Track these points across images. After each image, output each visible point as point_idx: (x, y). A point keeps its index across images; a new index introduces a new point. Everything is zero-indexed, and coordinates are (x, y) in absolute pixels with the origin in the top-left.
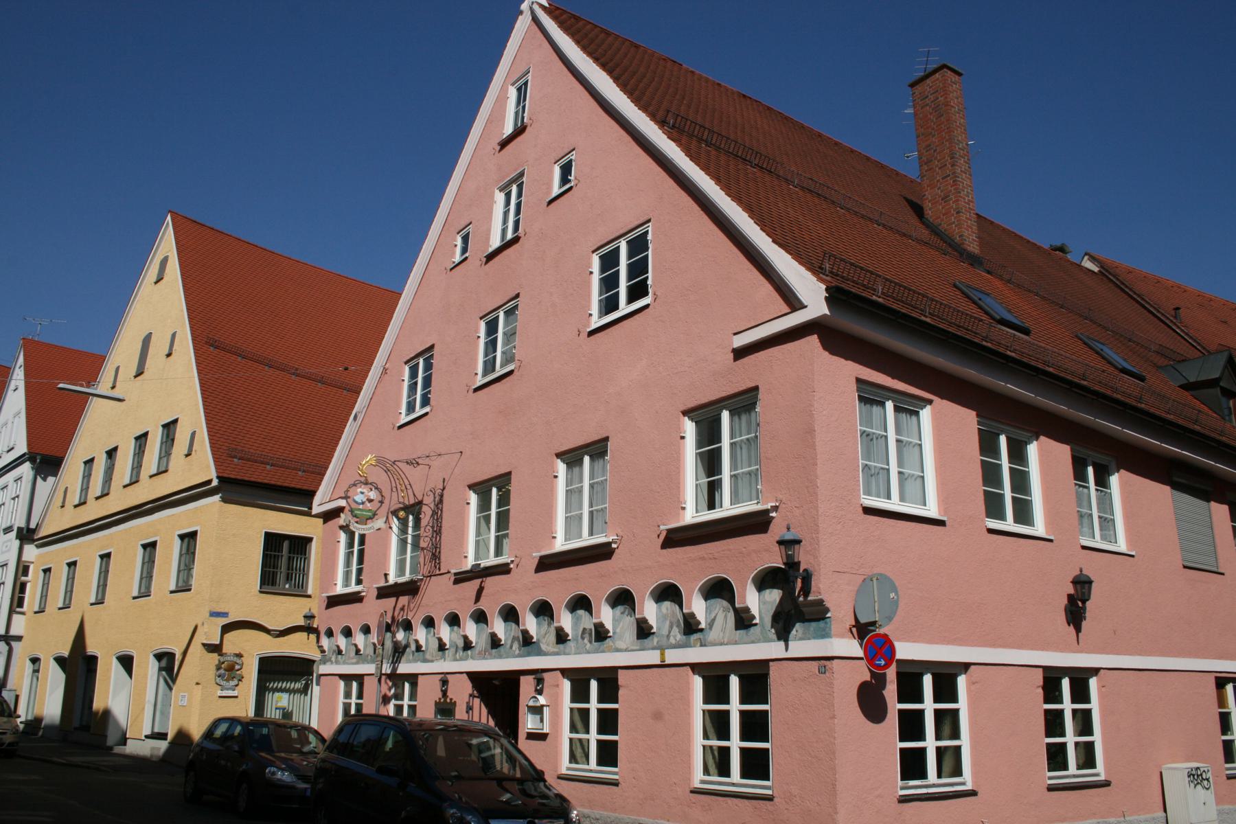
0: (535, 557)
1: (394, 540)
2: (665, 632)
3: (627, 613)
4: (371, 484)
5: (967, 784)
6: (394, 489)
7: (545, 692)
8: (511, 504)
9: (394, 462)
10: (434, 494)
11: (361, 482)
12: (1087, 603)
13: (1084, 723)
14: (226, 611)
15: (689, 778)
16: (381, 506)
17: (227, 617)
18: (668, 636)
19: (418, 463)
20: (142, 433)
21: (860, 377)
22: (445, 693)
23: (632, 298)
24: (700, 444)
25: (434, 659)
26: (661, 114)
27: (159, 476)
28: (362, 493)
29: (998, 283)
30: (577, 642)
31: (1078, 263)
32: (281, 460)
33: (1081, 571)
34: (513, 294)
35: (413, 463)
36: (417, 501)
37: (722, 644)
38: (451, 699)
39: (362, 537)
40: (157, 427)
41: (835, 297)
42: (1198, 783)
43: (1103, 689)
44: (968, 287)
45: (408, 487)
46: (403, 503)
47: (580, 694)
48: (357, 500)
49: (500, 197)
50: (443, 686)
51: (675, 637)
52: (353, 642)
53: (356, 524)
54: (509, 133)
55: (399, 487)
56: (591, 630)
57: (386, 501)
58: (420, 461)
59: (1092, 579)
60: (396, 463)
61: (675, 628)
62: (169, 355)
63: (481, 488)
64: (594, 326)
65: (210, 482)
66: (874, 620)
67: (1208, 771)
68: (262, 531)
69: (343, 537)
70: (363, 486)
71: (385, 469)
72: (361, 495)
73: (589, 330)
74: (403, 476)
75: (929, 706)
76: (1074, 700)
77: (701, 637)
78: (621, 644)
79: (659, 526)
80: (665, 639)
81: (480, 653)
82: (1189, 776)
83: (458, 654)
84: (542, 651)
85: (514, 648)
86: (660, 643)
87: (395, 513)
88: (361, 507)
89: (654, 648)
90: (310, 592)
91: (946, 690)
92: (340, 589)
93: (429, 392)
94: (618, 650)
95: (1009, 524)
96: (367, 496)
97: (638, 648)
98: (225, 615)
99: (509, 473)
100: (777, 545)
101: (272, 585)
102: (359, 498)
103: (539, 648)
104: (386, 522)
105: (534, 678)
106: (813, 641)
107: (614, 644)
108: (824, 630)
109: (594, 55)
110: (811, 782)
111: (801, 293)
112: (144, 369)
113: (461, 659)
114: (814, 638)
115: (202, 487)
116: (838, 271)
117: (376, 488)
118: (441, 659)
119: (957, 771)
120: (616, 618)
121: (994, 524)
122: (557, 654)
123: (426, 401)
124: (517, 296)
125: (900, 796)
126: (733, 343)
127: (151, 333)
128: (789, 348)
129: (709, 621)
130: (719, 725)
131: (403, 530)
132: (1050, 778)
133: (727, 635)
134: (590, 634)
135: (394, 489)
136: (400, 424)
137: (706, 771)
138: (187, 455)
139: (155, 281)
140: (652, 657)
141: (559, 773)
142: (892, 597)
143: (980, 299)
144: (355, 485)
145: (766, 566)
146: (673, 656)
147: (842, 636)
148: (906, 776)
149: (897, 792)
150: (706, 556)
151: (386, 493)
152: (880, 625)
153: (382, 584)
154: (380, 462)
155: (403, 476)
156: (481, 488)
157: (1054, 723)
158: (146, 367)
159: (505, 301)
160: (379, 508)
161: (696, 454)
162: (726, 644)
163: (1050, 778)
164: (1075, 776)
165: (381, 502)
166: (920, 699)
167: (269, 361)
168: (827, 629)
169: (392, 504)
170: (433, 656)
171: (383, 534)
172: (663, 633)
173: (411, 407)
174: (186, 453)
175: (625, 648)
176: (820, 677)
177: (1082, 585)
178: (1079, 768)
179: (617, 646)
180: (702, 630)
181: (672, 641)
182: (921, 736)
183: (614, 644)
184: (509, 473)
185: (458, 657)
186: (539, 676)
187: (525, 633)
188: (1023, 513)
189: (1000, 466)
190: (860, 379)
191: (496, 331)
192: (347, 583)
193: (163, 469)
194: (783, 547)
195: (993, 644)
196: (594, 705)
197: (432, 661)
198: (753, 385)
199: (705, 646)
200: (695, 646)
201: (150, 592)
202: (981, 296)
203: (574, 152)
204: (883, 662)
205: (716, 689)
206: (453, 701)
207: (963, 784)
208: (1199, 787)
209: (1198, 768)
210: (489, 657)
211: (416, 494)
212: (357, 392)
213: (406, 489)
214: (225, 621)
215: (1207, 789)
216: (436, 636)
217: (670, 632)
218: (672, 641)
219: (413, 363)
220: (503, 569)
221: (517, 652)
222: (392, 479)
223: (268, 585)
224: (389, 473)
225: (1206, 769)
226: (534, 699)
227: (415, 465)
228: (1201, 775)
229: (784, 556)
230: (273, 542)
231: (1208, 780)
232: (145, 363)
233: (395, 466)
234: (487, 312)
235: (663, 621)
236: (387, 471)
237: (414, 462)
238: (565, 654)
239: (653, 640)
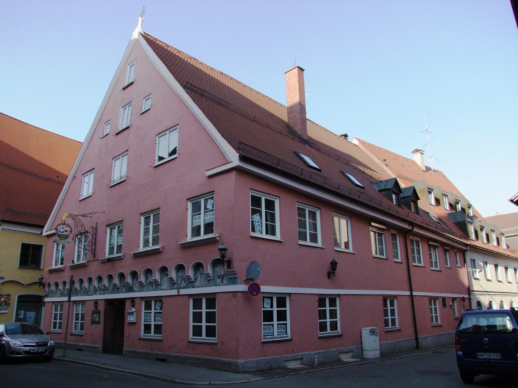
2: (179, 283)
3: (165, 275)
4: (67, 224)
5: (289, 337)
6: (76, 227)
8: (123, 232)
9: (76, 216)
10: (93, 229)
11: (62, 224)
12: (336, 271)
13: (333, 314)
15: (188, 337)
17: (4, 279)
18: (181, 284)
19: (86, 216)
22: (96, 307)
26: (185, 84)
28: (63, 228)
31: (351, 141)
32: (30, 213)
33: (334, 259)
34: (126, 150)
35: (84, 216)
36: (86, 231)
37: (200, 287)
41: (242, 158)
42: (373, 334)
43: (341, 302)
45: (82, 226)
46: (80, 232)
48: (61, 231)
50: (132, 304)
51: (183, 284)
52: (103, 284)
53: (60, 241)
54: (126, 85)
55: (78, 225)
56: (152, 282)
57: (73, 231)
59: (337, 262)
60: (77, 216)
61: (183, 281)
63: (146, 215)
64: (156, 165)
66: (252, 278)
67: (377, 330)
74: (80, 221)
75: (328, 308)
76: (391, 306)
77: (192, 284)
78: (163, 287)
79: (177, 242)
80: (179, 285)
81: (110, 291)
82: (370, 332)
83: (101, 292)
84: (134, 290)
85: (123, 290)
88: (62, 234)
89: (175, 289)
91: (333, 302)
94: (162, 290)
95: (308, 243)
102: (62, 230)
104: (73, 240)
109: (161, 57)
113: (103, 294)
116: (249, 148)
117: (69, 226)
118: (95, 294)
121: (301, 242)
122: (140, 291)
125: (263, 342)
126: (206, 174)
130: (197, 317)
131: (147, 223)
132: (320, 334)
133: (202, 283)
134: (152, 284)
135: (76, 227)
141: (140, 337)
144: (60, 225)
146: (183, 292)
147: (241, 284)
149: (262, 340)
151: (73, 228)
154: (70, 216)
155: (80, 221)
156: (146, 215)
157: (322, 315)
160: (70, 234)
162: (201, 287)
163: (320, 334)
164: (329, 333)
165: (71, 232)
167: (25, 171)
169: (75, 232)
170: (92, 293)
175: (165, 289)
177: (334, 264)
178: (331, 330)
179: (162, 288)
181: (182, 286)
187: (171, 279)
188: (314, 238)
192: (56, 265)
194: (220, 251)
195: (301, 286)
197: (91, 295)
199: (194, 288)
200: (190, 288)
203: (151, 95)
204: (256, 293)
205: (197, 304)
207: (287, 337)
208: (374, 335)
209: (373, 329)
211: (85, 228)
212: (64, 184)
213: (81, 226)
214: (2, 281)
215: (376, 336)
216: (93, 285)
217: (181, 282)
218: (182, 286)
220: (119, 259)
221: (125, 291)
224: (74, 220)
225: (376, 329)
226: (130, 309)
227: (85, 217)
228: (375, 331)
229: (221, 254)
231: (377, 333)
233: (77, 217)
238: (143, 291)
239: (175, 286)
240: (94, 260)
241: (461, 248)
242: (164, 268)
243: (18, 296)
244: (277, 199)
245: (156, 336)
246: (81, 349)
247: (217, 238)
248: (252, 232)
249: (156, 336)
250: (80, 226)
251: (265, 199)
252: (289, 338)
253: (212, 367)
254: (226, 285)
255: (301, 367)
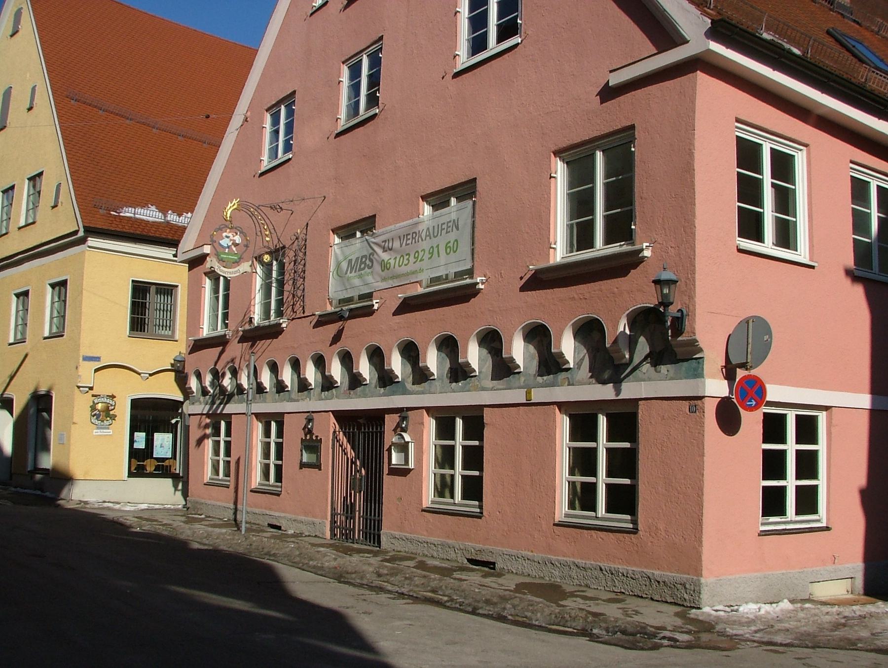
0: (400, 298)
1: (258, 282)
7: (410, 428)
14: (98, 355)
16: (246, 250)
20: (9, 186)
21: (739, 117)
23: (501, 39)
24: (572, 184)
25: (300, 398)
27: (27, 227)
28: (228, 237)
29: (867, 34)
30: (443, 381)
34: (376, 38)
38: (317, 437)
39: (227, 282)
40: (24, 181)
44: (843, 35)
45: (272, 231)
47: (445, 430)
48: (222, 244)
49: (268, 119)
58: (283, 206)
62: (30, 109)
65: (76, 232)
68: (129, 280)
69: (208, 283)
70: (228, 230)
71: (250, 213)
72: (228, 239)
73: (455, 71)
77: (569, 376)
86: (526, 382)
87: (259, 259)
90: (177, 338)
92: (205, 332)
93: (292, 138)
96: (231, 240)
97: (505, 387)
98: (97, 359)
99: (375, 216)
100: (653, 284)
101: (141, 331)
103: (404, 387)
104: (251, 266)
105: (399, 416)
106: (684, 381)
107: (480, 383)
108: (695, 370)
110: (678, 517)
111: (680, 24)
112: (6, 123)
113: (326, 399)
114: (686, 378)
115: (72, 237)
119: (814, 510)
120: (483, 358)
123: (288, 148)
124: (381, 38)
127: (11, 87)
128: (669, 86)
129: (577, 360)
135: (259, 234)
136: (262, 171)
137: (572, 506)
138: (53, 207)
139: (10, 33)
140: (518, 396)
142: (765, 339)
143: (854, 46)
145: (639, 306)
146: (538, 395)
147: (713, 377)
148: (766, 512)
150: (576, 296)
152: (751, 367)
153: (247, 327)
158: (8, 122)
159: (368, 44)
161: (568, 194)
165: (247, 246)
166: (783, 441)
168: (700, 369)
171: (247, 277)
172: (530, 372)
173: (274, 152)
174: (53, 204)
176: (690, 415)
180: (568, 369)
182: (782, 476)
183: (480, 383)
184: (375, 216)
185: (323, 397)
186: (404, 414)
189: (869, 215)
190: (739, 119)
191: (359, 75)
193: (31, 221)
196: (459, 442)
197: (298, 401)
198: (629, 124)
199: (573, 385)
201: (26, 339)
202: (854, 43)
206: (319, 438)
210: (353, 396)
219: (275, 110)
222: (257, 225)
223: (137, 331)
227: (279, 210)
230: (140, 290)
232: (7, 117)
234: (349, 56)
235: (531, 360)
236: (252, 215)
237: (278, 207)
239: (519, 379)
240: (303, 315)
241: (50, 444)
242: (489, 333)
243: (132, 400)
244: (801, 150)
245: (467, 506)
246: (278, 525)
247: (645, 251)
248: (739, 237)
249: (467, 506)
250: (267, 233)
251: (771, 148)
252: (824, 525)
253: (623, 591)
254: (669, 377)
255: (851, 599)
